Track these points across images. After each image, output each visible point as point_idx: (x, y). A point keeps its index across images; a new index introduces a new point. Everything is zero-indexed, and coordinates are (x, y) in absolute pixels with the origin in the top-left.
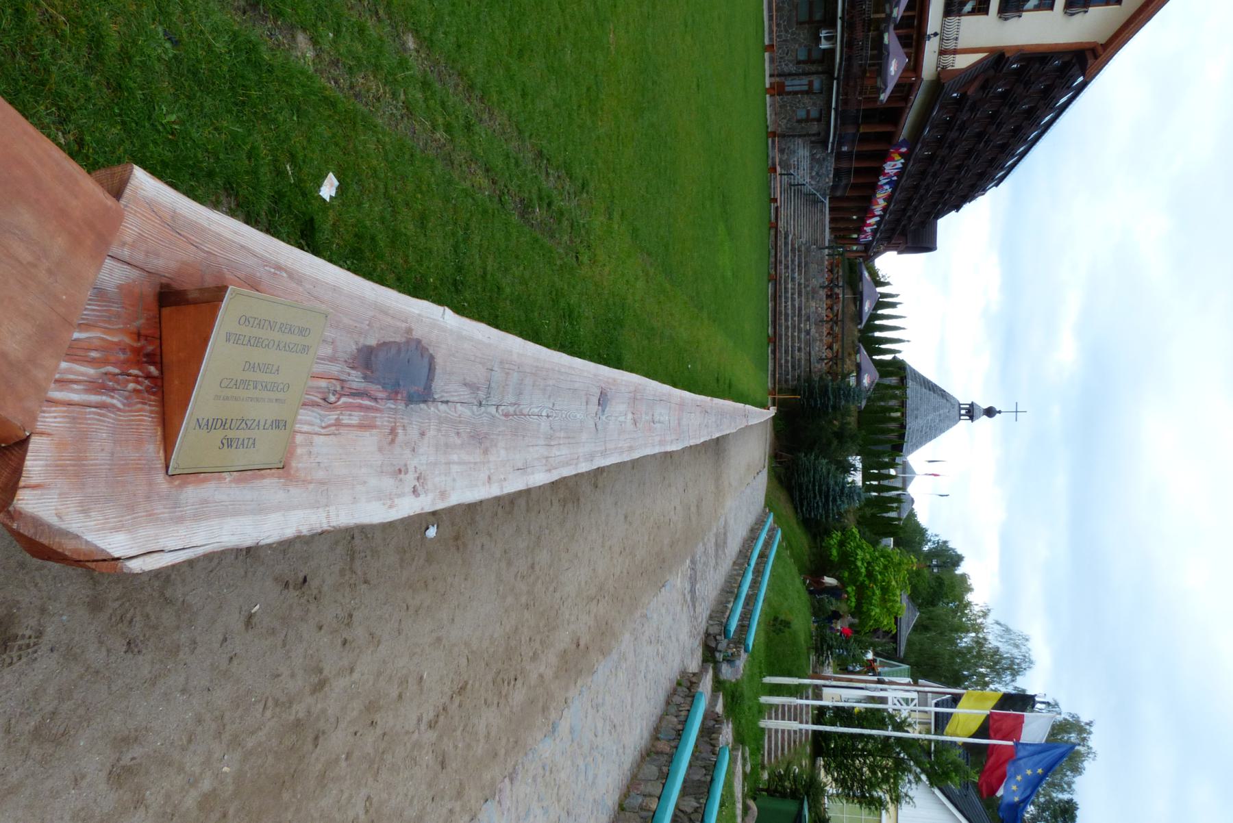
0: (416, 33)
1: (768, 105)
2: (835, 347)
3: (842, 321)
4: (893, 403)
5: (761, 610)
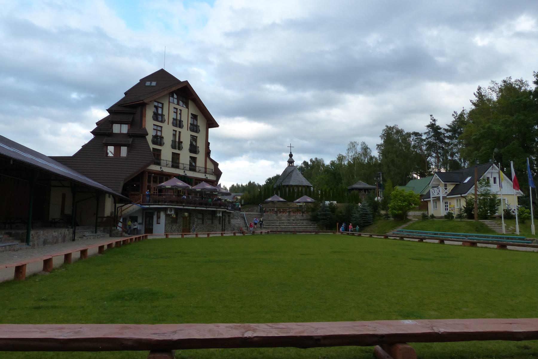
5: (533, 211)
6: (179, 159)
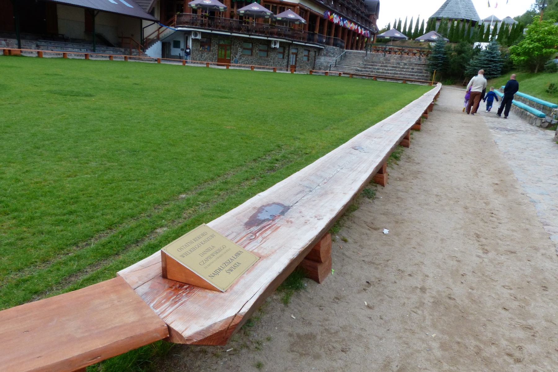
0: (180, 193)
1: (299, 73)
2: (415, 51)
3: (402, 47)
4: (449, 25)
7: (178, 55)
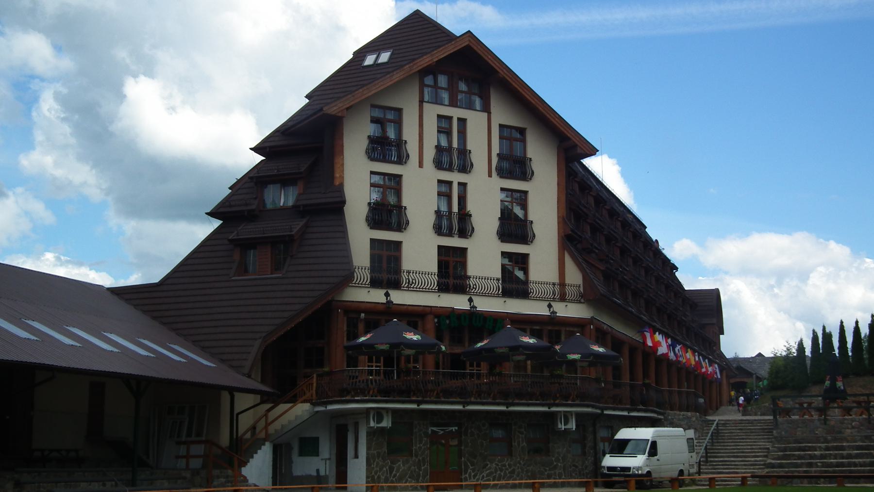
6: (464, 264)
7: (315, 474)
